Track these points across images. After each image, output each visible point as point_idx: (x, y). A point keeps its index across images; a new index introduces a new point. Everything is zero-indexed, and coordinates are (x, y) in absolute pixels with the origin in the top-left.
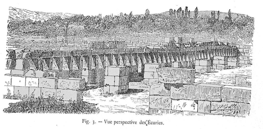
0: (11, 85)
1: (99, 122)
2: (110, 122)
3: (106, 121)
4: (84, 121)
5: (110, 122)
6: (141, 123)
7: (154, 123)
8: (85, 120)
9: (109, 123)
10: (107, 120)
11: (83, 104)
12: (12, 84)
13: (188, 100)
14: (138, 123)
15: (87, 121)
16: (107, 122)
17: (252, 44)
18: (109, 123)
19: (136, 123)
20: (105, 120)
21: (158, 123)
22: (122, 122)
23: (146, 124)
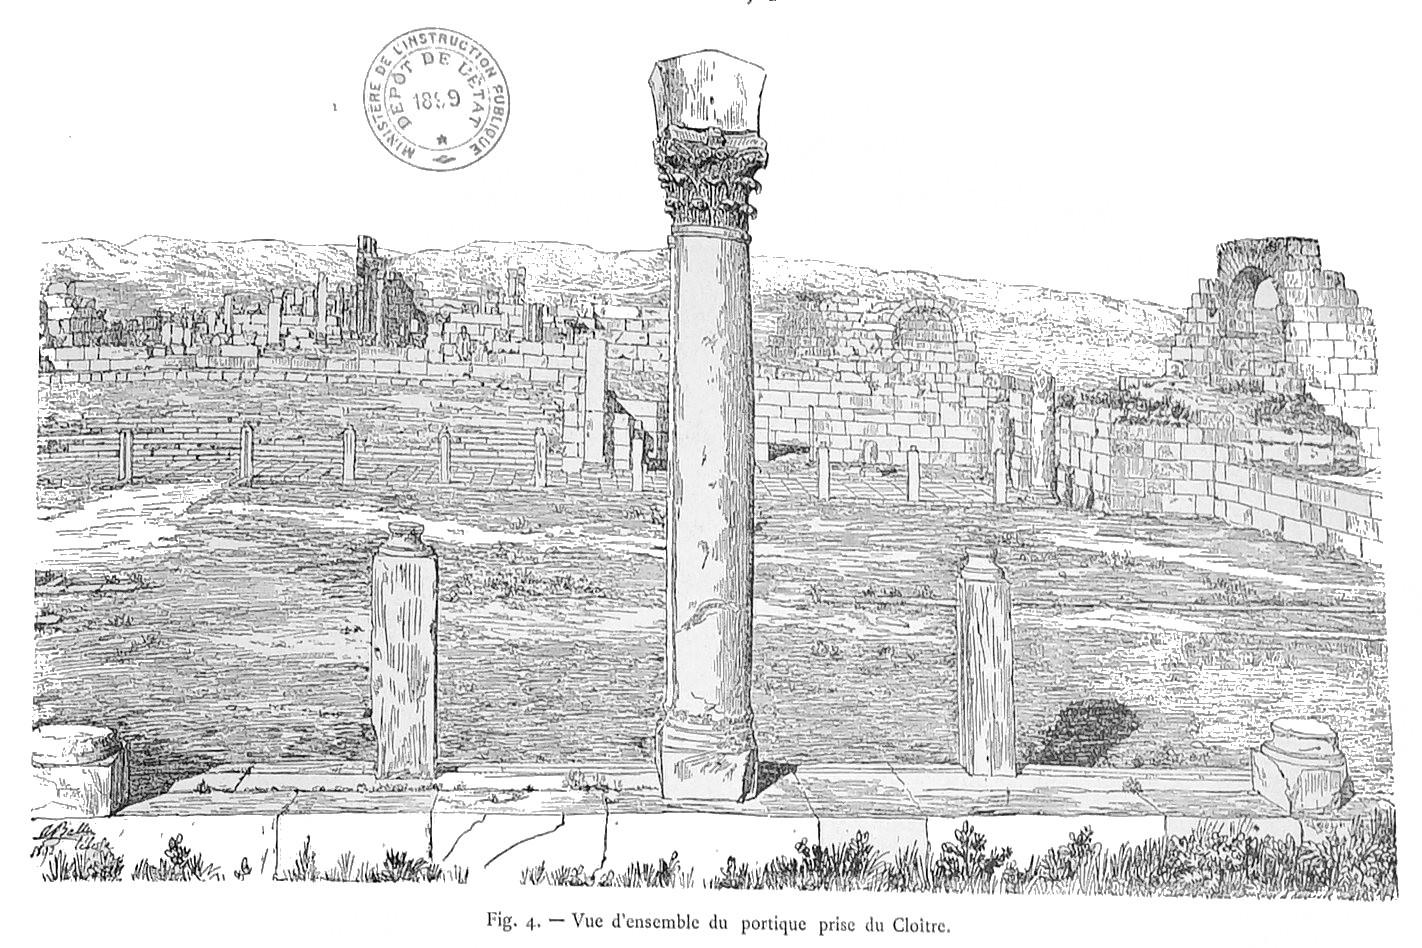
0: (1042, 414)
1: (562, 920)
2: (597, 923)
3: (578, 917)
4: (494, 919)
5: (597, 923)
6: (869, 928)
7: (793, 927)
8: (497, 916)
9: (590, 924)
10: (582, 914)
11: (346, 333)
12: (1041, 412)
13: (959, 279)
14: (704, 924)
15: (507, 920)
16: (584, 919)
17: (1362, 556)
18: (590, 924)
19: (849, 927)
20: (575, 915)
21: (798, 927)
22: (644, 924)
23: (626, 918)
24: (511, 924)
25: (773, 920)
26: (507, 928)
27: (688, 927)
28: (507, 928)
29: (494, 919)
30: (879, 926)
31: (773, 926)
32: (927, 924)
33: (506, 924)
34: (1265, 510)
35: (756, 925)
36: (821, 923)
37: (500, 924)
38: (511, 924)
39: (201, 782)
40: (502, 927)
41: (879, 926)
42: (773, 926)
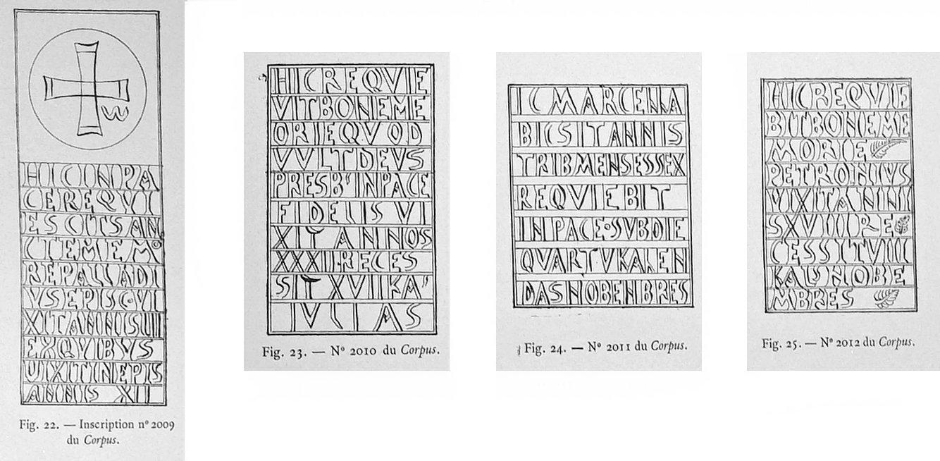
8: (769, 342)
15: (276, 352)
22: (90, 426)
24: (35, 427)
25: (118, 421)
26: (776, 349)
27: (366, 349)
28: (776, 349)
29: (767, 343)
30: (872, 342)
31: (118, 425)
32: (391, 349)
33: (774, 346)
34: (534, 186)
35: (125, 425)
36: (140, 423)
37: (534, 351)
38: (35, 427)
39: (581, 265)
40: (535, 353)
41: (872, 342)
42: (118, 425)
